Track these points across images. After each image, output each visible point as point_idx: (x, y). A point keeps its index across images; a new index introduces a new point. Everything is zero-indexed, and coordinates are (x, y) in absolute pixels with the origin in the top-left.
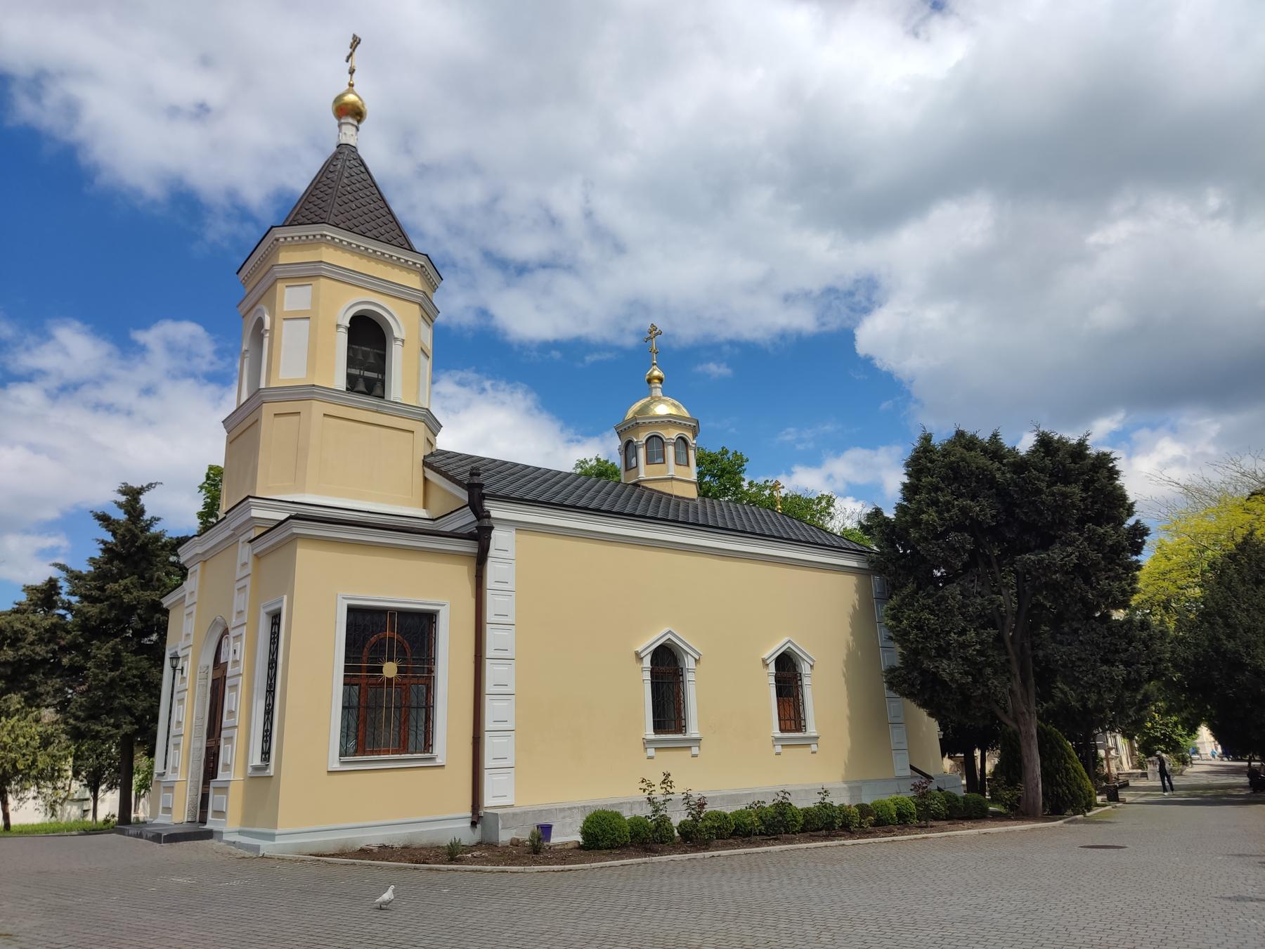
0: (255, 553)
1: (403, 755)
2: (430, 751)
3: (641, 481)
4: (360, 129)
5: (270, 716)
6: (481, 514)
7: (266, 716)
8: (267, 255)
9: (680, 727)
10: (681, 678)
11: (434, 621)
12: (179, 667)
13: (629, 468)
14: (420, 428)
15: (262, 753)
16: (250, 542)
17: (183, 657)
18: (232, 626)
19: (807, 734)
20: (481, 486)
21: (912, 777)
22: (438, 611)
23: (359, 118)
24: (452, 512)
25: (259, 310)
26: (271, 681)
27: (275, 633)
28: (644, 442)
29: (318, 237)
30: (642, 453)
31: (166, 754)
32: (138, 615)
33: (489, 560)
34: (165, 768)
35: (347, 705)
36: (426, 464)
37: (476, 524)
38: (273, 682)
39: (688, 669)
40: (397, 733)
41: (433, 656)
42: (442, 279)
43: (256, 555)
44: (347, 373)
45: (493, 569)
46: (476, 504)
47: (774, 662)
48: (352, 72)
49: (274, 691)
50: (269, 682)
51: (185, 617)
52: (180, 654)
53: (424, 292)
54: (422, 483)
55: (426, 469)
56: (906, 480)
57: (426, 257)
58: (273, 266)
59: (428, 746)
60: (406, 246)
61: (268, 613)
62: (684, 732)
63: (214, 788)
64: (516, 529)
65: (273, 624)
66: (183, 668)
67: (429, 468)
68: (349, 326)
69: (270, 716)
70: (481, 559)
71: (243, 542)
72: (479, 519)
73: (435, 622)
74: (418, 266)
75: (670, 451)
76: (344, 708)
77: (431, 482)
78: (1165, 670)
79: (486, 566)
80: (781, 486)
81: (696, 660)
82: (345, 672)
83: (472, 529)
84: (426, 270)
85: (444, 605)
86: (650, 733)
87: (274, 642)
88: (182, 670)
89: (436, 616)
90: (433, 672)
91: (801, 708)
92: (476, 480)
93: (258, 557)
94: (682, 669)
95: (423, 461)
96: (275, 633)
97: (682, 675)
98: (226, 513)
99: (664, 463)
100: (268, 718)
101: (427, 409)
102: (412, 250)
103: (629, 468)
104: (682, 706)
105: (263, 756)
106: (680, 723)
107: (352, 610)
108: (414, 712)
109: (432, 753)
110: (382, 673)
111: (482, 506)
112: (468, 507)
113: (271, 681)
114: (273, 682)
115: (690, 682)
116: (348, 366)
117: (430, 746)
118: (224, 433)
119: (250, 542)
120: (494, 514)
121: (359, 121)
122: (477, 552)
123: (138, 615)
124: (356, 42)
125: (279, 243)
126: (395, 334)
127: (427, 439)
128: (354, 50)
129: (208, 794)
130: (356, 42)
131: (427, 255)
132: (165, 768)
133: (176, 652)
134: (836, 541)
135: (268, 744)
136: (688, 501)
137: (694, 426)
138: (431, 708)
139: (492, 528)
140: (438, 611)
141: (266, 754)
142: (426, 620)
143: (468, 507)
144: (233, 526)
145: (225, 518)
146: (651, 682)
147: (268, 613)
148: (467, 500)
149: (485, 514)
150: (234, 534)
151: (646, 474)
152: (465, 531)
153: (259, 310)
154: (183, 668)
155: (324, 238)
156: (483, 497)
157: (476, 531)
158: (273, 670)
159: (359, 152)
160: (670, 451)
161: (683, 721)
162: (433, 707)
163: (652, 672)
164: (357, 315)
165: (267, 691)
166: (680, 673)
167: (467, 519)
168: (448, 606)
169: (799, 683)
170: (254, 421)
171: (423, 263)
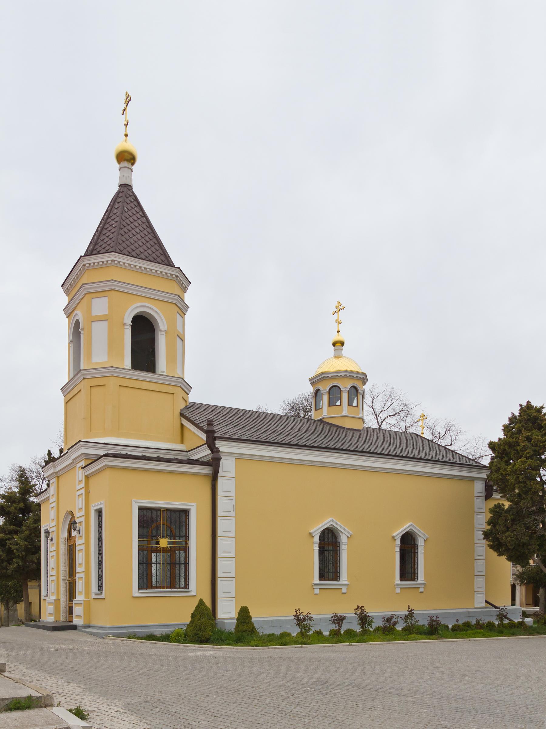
0: (86, 474)
2: (188, 588)
3: (324, 418)
5: (101, 567)
6: (214, 449)
7: (99, 567)
8: (78, 275)
9: (336, 576)
10: (338, 548)
11: (188, 515)
12: (50, 538)
13: (317, 409)
14: (179, 393)
15: (99, 586)
16: (83, 468)
17: (51, 532)
18: (77, 516)
19: (341, 582)
20: (214, 432)
22: (190, 509)
23: (132, 162)
24: (198, 447)
25: (76, 314)
26: (100, 548)
27: (100, 561)
28: (328, 390)
29: (110, 262)
30: (326, 398)
31: (47, 585)
33: (219, 478)
34: (47, 593)
35: (141, 562)
36: (182, 415)
37: (211, 456)
38: (101, 548)
39: (343, 543)
40: (169, 578)
41: (188, 535)
42: (190, 283)
43: (86, 476)
45: (221, 484)
46: (211, 440)
47: (400, 538)
48: (126, 125)
49: (102, 553)
50: (99, 535)
51: (50, 509)
52: (50, 530)
53: (179, 296)
54: (180, 427)
55: (182, 419)
56: (517, 413)
57: (179, 269)
58: (83, 284)
59: (186, 586)
60: (166, 262)
61: (96, 510)
62: (416, 579)
63: (75, 604)
64: (236, 458)
65: (98, 516)
67: (183, 418)
68: (131, 324)
69: (101, 567)
70: (214, 478)
71: (79, 468)
72: (213, 452)
73: (188, 516)
74: (174, 276)
75: (345, 396)
76: (139, 563)
77: (186, 427)
78: (14, 585)
79: (217, 483)
80: (425, 417)
81: (348, 537)
82: (139, 544)
83: (209, 458)
84: (179, 278)
85: (193, 506)
86: (317, 581)
87: (100, 540)
88: (52, 539)
89: (189, 512)
90: (188, 544)
91: (416, 566)
92: (210, 428)
93: (87, 477)
94: (339, 542)
95: (180, 413)
96: (100, 561)
97: (339, 546)
98: (68, 450)
100: (100, 568)
101: (182, 378)
103: (317, 409)
104: (338, 564)
105: (99, 588)
106: (415, 575)
107: (141, 509)
108: (177, 566)
109: (189, 589)
110: (159, 545)
111: (214, 445)
112: (206, 445)
113: (100, 548)
114: (101, 548)
115: (344, 551)
117: (187, 585)
118: (62, 397)
119: (83, 468)
120: (221, 449)
121: (133, 164)
122: (212, 473)
124: (128, 100)
125: (86, 267)
126: (160, 327)
128: (127, 106)
129: (72, 607)
130: (128, 100)
131: (179, 268)
132: (47, 593)
133: (47, 529)
135: (101, 581)
137: (363, 378)
138: (188, 564)
139: (221, 458)
140: (190, 509)
141: (100, 587)
142: (185, 513)
143: (206, 445)
144: (73, 457)
145: (67, 453)
146: (319, 550)
147: (96, 510)
148: (205, 439)
149: (216, 450)
151: (328, 413)
152: (205, 460)
153: (76, 314)
154: (52, 538)
155: (113, 263)
156: (215, 439)
157: (211, 460)
158: (101, 528)
159: (134, 190)
160: (345, 396)
161: (338, 573)
162: (188, 564)
163: (319, 544)
165: (98, 553)
166: (338, 545)
167: (205, 453)
168: (195, 506)
169: (416, 551)
171: (177, 274)
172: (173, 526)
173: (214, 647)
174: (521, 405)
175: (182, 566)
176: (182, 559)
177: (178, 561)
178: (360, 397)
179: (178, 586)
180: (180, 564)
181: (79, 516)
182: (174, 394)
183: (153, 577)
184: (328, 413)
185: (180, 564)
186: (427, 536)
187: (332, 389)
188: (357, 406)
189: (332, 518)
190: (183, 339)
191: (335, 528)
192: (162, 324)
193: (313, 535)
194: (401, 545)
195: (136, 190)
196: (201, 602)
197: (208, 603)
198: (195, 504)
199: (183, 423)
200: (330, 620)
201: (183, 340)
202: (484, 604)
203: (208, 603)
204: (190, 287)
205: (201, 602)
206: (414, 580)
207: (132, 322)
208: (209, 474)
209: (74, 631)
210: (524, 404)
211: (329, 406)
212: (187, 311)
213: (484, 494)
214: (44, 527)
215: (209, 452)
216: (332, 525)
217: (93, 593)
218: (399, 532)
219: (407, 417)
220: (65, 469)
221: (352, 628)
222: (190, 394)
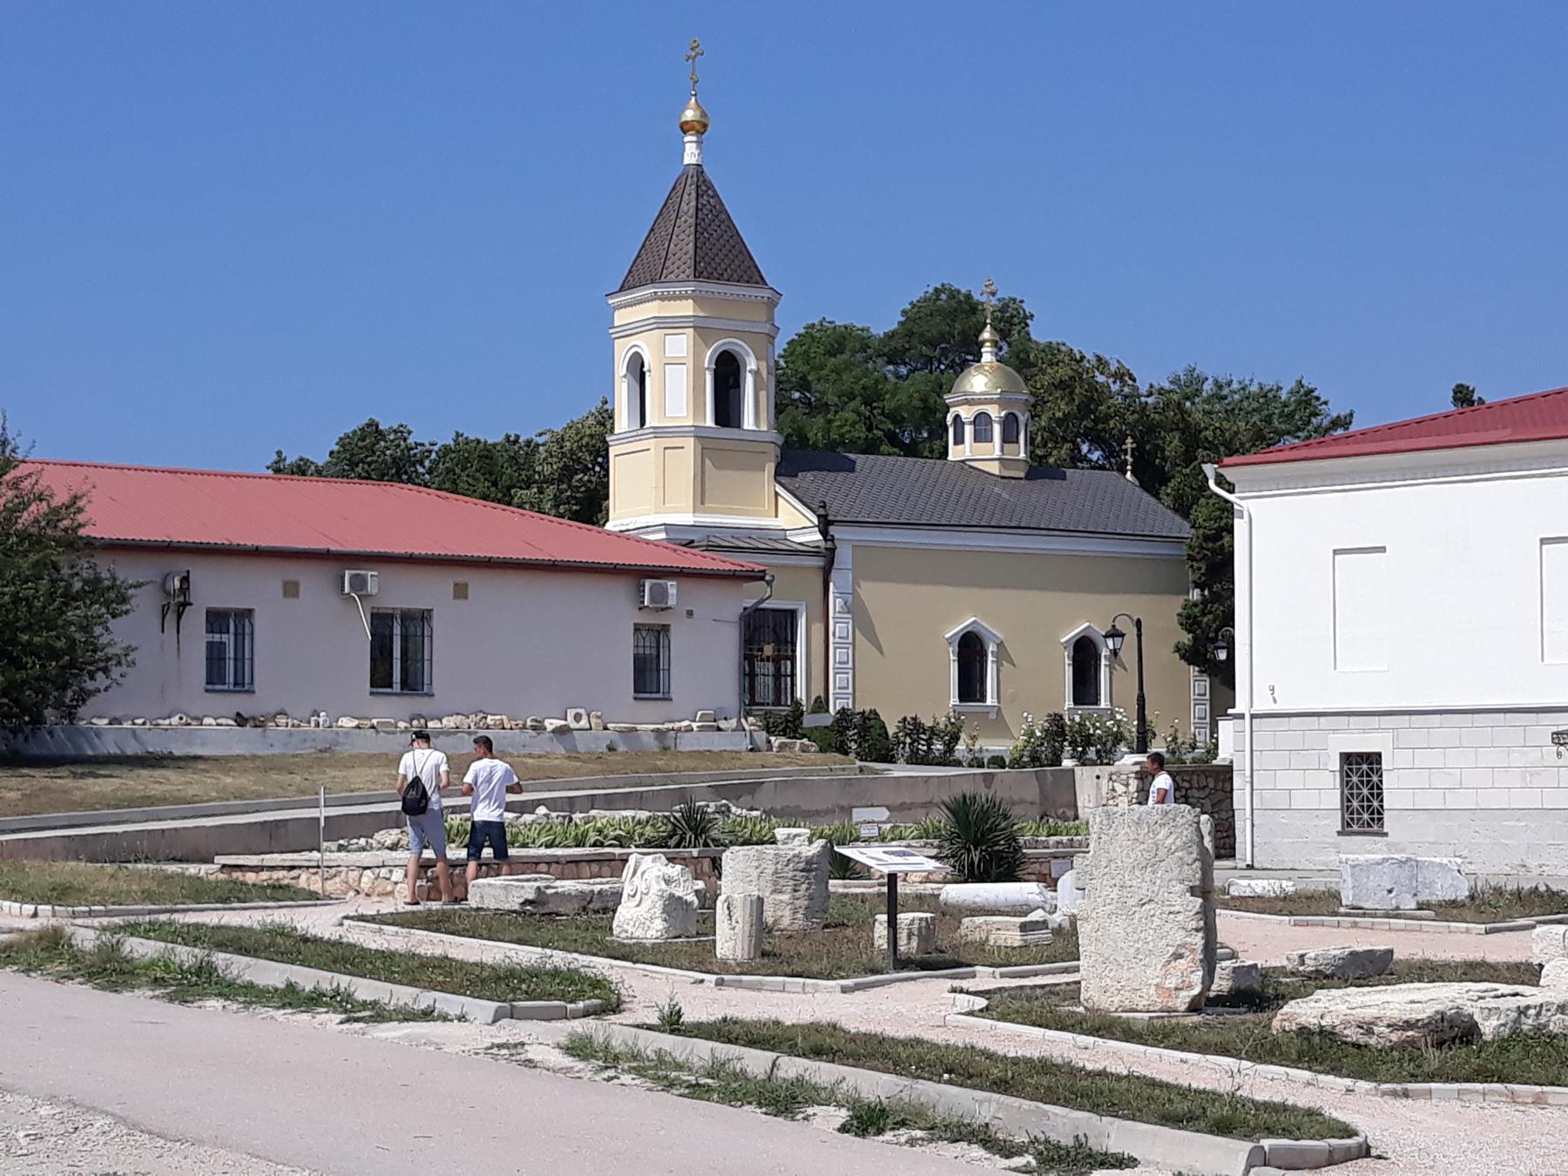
55: (777, 485)
72: (825, 540)
108: (783, 679)
120: (836, 536)
173: (740, 981)
175: (789, 679)
176: (789, 672)
177: (783, 673)
179: (783, 703)
180: (786, 676)
183: (223, 922)
185: (786, 676)
186: (999, 635)
189: (973, 619)
199: (778, 490)
200: (1078, 889)
206: (1096, 704)
207: (716, 364)
215: (819, 537)
218: (955, 630)
219: (193, 1144)
221: (1312, 1104)
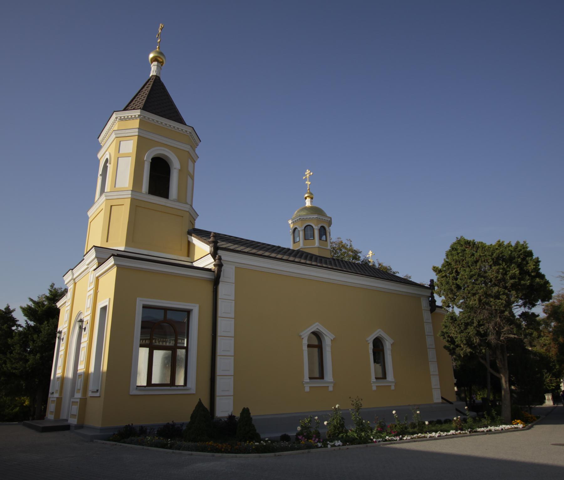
1: (172, 387)
4: (162, 69)
21: (442, 403)
24: (201, 258)
28: (303, 228)
30: (301, 234)
32: (551, 327)
33: (220, 282)
39: (327, 345)
42: (201, 141)
44: (211, 232)
47: (372, 342)
66: (63, 338)
68: (151, 161)
99: (314, 239)
102: (186, 125)
112: (210, 255)
116: (215, 233)
123: (551, 327)
127: (190, 221)
134: (398, 279)
136: (326, 259)
140: (192, 310)
150: (88, 268)
154: (63, 338)
164: (155, 157)
170: (101, 209)
171: (190, 131)
172: (120, 138)
174: (457, 238)
178: (328, 234)
181: (87, 317)
182: (183, 217)
184: (304, 244)
187: (307, 227)
188: (326, 241)
190: (193, 223)
191: (320, 331)
192: (176, 165)
193: (303, 337)
194: (373, 348)
195: (162, 79)
196: (200, 404)
197: (206, 404)
198: (198, 306)
201: (193, 179)
202: (440, 400)
203: (206, 404)
204: (200, 144)
205: (200, 404)
208: (210, 278)
209: (67, 432)
210: (459, 238)
211: (305, 239)
212: (197, 218)
213: (429, 308)
214: (59, 329)
216: (317, 329)
217: (90, 391)
220: (81, 275)
222: (197, 162)
